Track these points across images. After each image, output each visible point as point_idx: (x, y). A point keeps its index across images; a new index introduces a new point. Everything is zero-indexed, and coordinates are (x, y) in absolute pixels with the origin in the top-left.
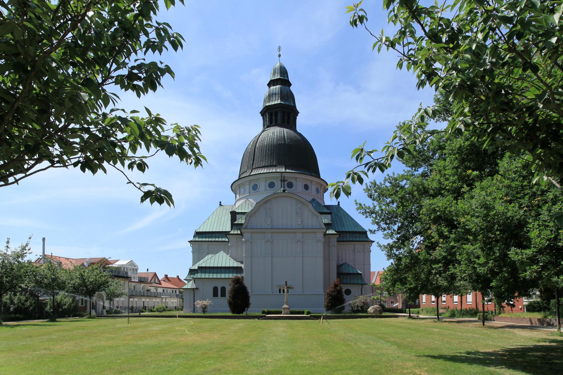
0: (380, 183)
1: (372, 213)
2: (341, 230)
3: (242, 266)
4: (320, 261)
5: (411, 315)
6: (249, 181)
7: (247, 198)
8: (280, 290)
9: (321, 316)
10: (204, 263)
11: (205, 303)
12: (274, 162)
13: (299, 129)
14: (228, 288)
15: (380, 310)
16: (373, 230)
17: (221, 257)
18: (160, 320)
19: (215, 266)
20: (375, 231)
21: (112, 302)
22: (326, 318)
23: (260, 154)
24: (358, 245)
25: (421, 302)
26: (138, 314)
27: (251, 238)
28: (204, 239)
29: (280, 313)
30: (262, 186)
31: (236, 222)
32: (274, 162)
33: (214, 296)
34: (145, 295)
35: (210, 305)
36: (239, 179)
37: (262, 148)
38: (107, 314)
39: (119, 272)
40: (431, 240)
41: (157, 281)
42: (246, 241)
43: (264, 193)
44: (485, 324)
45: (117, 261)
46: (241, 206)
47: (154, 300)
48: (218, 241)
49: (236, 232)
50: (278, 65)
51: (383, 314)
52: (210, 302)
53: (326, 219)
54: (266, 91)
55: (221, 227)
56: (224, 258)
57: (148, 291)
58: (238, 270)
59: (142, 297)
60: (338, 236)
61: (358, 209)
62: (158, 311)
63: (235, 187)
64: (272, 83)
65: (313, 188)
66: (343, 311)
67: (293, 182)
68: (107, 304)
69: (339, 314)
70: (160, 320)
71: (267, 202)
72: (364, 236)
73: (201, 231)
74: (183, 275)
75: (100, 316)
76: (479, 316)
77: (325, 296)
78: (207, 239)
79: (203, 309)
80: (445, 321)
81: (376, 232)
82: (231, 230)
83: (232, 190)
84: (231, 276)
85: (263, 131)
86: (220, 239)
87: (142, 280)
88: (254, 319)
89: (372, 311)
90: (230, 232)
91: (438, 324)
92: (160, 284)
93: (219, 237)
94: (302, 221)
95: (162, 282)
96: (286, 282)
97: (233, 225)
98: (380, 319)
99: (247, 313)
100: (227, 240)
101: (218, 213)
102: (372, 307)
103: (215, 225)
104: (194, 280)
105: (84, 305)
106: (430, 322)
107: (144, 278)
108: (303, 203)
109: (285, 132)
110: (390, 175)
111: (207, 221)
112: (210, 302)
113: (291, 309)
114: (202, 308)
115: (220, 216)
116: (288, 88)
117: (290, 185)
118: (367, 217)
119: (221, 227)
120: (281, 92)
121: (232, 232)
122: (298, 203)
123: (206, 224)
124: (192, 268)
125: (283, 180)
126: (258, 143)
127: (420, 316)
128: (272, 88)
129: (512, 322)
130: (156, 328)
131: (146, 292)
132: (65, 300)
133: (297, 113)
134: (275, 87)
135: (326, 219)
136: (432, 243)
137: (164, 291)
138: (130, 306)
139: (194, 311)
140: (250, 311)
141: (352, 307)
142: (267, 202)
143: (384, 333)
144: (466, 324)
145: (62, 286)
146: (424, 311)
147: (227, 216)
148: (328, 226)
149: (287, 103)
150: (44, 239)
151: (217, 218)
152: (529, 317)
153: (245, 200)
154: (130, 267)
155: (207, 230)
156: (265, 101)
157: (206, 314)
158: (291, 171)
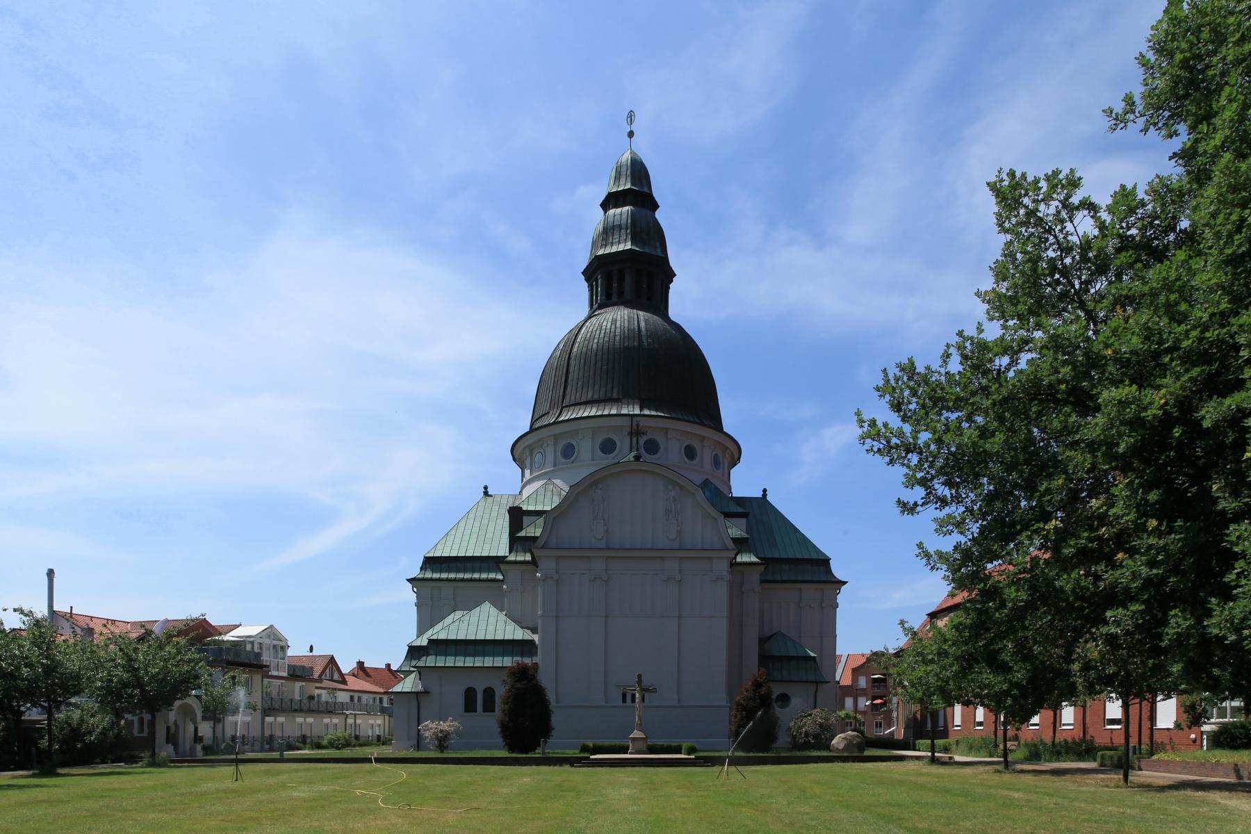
0: (928, 368)
1: (908, 451)
2: (770, 556)
3: (536, 638)
4: (721, 626)
5: (936, 754)
6: (555, 435)
7: (548, 476)
8: (624, 696)
9: (726, 758)
10: (441, 631)
11: (445, 726)
12: (615, 390)
13: (677, 310)
14: (501, 691)
15: (858, 743)
16: (912, 503)
17: (484, 616)
18: (325, 769)
19: (469, 638)
20: (916, 504)
21: (219, 727)
22: (735, 762)
23: (581, 371)
24: (809, 592)
25: (950, 726)
26: (276, 755)
27: (557, 570)
28: (444, 576)
29: (624, 750)
30: (586, 448)
31: (522, 534)
32: (615, 390)
33: (466, 710)
34: (305, 707)
35: (457, 731)
36: (532, 430)
37: (586, 356)
38: (206, 754)
39: (237, 654)
40: (1097, 529)
41: (336, 676)
42: (545, 579)
43: (588, 461)
44: (1130, 778)
45: (237, 626)
46: (534, 496)
47: (326, 720)
48: (480, 580)
49: (520, 558)
50: (627, 156)
51: (868, 753)
52: (457, 724)
53: (736, 530)
54: (596, 218)
55: (487, 547)
56: (492, 619)
57: (311, 698)
58: (524, 647)
59: (296, 714)
60: (762, 568)
61: (863, 438)
62: (332, 745)
63: (522, 451)
64: (611, 201)
65: (706, 456)
66: (774, 746)
67: (660, 438)
68: (205, 729)
69: (763, 752)
70: (325, 769)
71: (595, 483)
72: (822, 568)
73: (438, 554)
74: (397, 660)
75: (183, 759)
76: (1103, 757)
77: (731, 709)
78: (452, 576)
79: (440, 741)
80: (1022, 771)
81: (919, 509)
82: (510, 552)
83: (514, 460)
84: (508, 662)
85: (589, 317)
86: (484, 576)
87: (299, 673)
88: (561, 765)
89: (841, 746)
90: (507, 557)
91: (1007, 777)
92: (344, 682)
93: (480, 571)
94: (679, 532)
95: (350, 679)
96: (640, 676)
97: (515, 542)
98: (862, 764)
99: (543, 751)
100: (500, 577)
101: (480, 513)
102: (842, 735)
103: (473, 540)
104: (420, 673)
105: (145, 734)
106: (987, 772)
107: (304, 667)
108: (681, 487)
109: (642, 318)
110: (966, 334)
111: (454, 531)
112: (457, 724)
113: (652, 742)
114: (437, 738)
115: (485, 521)
116: (649, 212)
117: (652, 447)
118: (891, 462)
119: (487, 547)
120: (634, 223)
121: (512, 558)
122: (670, 487)
123: (451, 538)
124: (415, 644)
125: (635, 432)
126: (580, 337)
127: (958, 758)
128: (611, 212)
129: (1185, 774)
130: (303, 792)
131: (306, 701)
132: (92, 721)
133: (670, 275)
134: (618, 210)
135: (736, 530)
136: (1100, 538)
137: (352, 698)
138: (267, 733)
139: (418, 747)
140: (551, 748)
141: (794, 737)
142: (595, 483)
143: (889, 804)
144: (1078, 778)
145: (72, 685)
146: (963, 746)
147: (500, 521)
148: (741, 544)
149: (647, 251)
150: (51, 573)
151: (477, 524)
152: (1231, 760)
153: (544, 482)
154: (268, 641)
155: (454, 554)
156: (594, 244)
157: (445, 755)
158: (653, 413)
